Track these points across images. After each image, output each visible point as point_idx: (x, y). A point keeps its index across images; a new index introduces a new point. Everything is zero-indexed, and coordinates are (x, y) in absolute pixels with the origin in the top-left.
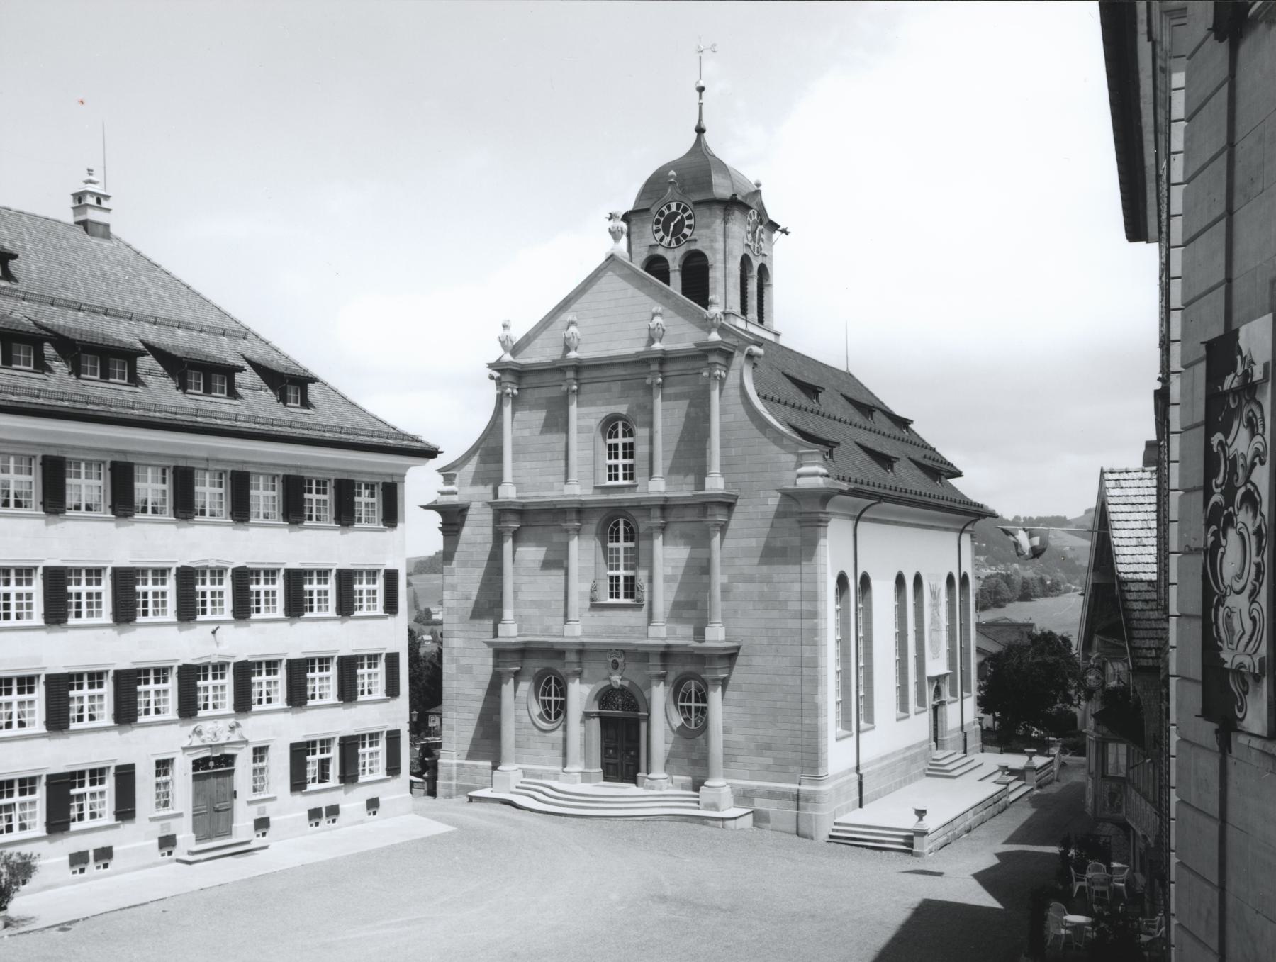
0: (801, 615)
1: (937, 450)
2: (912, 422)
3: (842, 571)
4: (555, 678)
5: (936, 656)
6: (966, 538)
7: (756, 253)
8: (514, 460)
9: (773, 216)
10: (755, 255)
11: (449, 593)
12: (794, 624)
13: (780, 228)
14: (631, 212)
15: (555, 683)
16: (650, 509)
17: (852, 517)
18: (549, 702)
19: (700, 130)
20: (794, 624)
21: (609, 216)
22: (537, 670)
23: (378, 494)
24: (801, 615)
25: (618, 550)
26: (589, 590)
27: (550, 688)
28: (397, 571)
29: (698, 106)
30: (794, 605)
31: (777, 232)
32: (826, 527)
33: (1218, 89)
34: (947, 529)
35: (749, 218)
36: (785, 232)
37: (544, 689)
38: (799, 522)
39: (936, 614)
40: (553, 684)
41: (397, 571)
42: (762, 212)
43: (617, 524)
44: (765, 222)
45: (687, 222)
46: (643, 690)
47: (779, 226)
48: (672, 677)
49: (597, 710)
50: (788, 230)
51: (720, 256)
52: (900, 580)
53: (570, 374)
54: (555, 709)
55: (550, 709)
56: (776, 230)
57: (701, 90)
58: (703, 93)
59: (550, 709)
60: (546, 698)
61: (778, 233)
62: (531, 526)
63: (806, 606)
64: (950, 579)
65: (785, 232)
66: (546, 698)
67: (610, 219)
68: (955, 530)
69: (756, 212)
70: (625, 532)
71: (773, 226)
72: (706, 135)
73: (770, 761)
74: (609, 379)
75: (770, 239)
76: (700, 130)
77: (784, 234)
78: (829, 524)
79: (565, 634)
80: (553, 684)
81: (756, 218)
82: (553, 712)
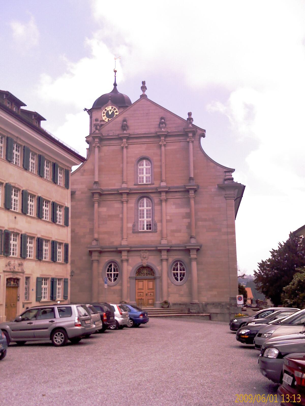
0: (227, 233)
2: (233, 171)
12: (224, 237)
16: (161, 193)
18: (177, 274)
19: (115, 85)
20: (224, 237)
22: (107, 260)
24: (227, 233)
25: (143, 210)
26: (132, 226)
30: (224, 230)
37: (108, 269)
38: (225, 198)
40: (179, 265)
45: (115, 111)
48: (171, 260)
49: (134, 276)
53: (125, 140)
55: (178, 277)
57: (115, 71)
62: (104, 201)
63: (229, 230)
76: (115, 85)
80: (179, 265)
82: (113, 279)
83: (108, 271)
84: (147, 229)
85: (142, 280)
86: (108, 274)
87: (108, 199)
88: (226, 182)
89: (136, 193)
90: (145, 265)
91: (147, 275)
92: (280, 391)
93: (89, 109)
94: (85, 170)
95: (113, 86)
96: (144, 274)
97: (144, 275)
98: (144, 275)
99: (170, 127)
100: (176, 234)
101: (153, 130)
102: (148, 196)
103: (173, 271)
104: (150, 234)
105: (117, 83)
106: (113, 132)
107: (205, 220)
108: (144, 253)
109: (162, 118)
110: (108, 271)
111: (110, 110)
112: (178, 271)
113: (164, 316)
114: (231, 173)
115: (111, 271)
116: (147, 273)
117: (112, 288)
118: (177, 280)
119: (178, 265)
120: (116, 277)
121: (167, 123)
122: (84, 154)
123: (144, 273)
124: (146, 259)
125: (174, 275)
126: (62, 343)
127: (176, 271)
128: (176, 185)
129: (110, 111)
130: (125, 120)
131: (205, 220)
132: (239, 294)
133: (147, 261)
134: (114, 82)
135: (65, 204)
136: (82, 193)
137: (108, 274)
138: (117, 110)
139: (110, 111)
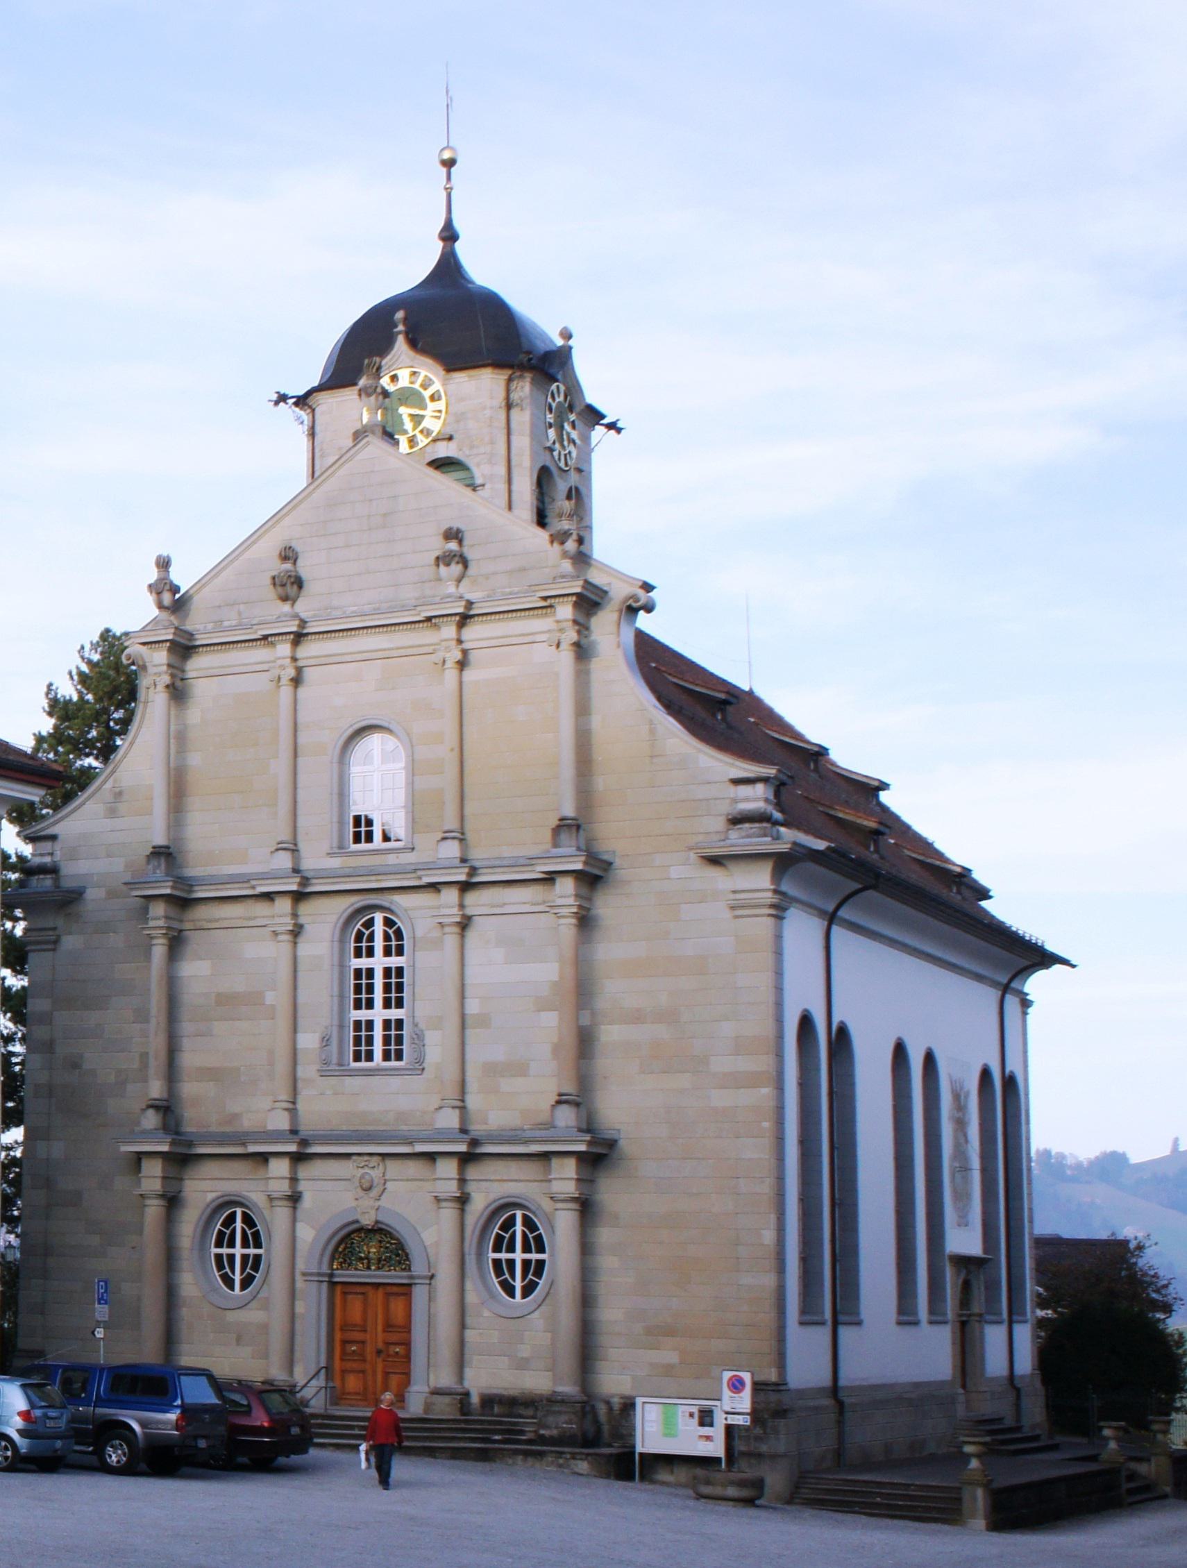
2: (884, 786)
3: (806, 1010)
5: (963, 1222)
7: (562, 464)
9: (592, 397)
10: (560, 469)
13: (605, 421)
17: (821, 913)
19: (449, 235)
21: (275, 397)
22: (210, 1196)
27: (234, 1232)
29: (444, 194)
31: (597, 427)
33: (596, 445)
34: (979, 978)
35: (550, 400)
39: (962, 1140)
42: (574, 389)
43: (370, 924)
44: (578, 408)
46: (419, 1229)
47: (602, 417)
50: (619, 425)
52: (900, 1051)
56: (598, 424)
57: (449, 164)
58: (453, 170)
59: (233, 1271)
61: (599, 431)
64: (986, 1074)
65: (164, 564)
67: (277, 403)
68: (994, 984)
69: (562, 388)
70: (387, 937)
71: (594, 416)
72: (458, 245)
73: (672, 1357)
74: (359, 657)
75: (586, 439)
76: (449, 235)
77: (612, 432)
81: (562, 398)
84: (387, 1056)
85: (359, 1289)
87: (217, 920)
90: (367, 1221)
91: (378, 1268)
92: (523, 1428)
93: (301, 392)
94: (120, 794)
95: (439, 246)
96: (369, 1262)
97: (369, 1268)
98: (369, 1268)
99: (487, 577)
100: (507, 1085)
101: (409, 594)
102: (386, 904)
104: (395, 1082)
105: (457, 225)
106: (240, 613)
107: (637, 1017)
108: (366, 1170)
109: (453, 535)
110: (219, 1244)
111: (417, 419)
115: (245, 1258)
116: (379, 1260)
117: (232, 1317)
119: (514, 1225)
120: (252, 1269)
121: (469, 553)
123: (367, 1258)
124: (374, 1193)
126: (8, 1465)
128: (508, 852)
129: (412, 416)
130: (288, 555)
131: (637, 1017)
133: (378, 1204)
134: (441, 224)
136: (112, 894)
137: (219, 1257)
138: (437, 386)
139: (412, 416)
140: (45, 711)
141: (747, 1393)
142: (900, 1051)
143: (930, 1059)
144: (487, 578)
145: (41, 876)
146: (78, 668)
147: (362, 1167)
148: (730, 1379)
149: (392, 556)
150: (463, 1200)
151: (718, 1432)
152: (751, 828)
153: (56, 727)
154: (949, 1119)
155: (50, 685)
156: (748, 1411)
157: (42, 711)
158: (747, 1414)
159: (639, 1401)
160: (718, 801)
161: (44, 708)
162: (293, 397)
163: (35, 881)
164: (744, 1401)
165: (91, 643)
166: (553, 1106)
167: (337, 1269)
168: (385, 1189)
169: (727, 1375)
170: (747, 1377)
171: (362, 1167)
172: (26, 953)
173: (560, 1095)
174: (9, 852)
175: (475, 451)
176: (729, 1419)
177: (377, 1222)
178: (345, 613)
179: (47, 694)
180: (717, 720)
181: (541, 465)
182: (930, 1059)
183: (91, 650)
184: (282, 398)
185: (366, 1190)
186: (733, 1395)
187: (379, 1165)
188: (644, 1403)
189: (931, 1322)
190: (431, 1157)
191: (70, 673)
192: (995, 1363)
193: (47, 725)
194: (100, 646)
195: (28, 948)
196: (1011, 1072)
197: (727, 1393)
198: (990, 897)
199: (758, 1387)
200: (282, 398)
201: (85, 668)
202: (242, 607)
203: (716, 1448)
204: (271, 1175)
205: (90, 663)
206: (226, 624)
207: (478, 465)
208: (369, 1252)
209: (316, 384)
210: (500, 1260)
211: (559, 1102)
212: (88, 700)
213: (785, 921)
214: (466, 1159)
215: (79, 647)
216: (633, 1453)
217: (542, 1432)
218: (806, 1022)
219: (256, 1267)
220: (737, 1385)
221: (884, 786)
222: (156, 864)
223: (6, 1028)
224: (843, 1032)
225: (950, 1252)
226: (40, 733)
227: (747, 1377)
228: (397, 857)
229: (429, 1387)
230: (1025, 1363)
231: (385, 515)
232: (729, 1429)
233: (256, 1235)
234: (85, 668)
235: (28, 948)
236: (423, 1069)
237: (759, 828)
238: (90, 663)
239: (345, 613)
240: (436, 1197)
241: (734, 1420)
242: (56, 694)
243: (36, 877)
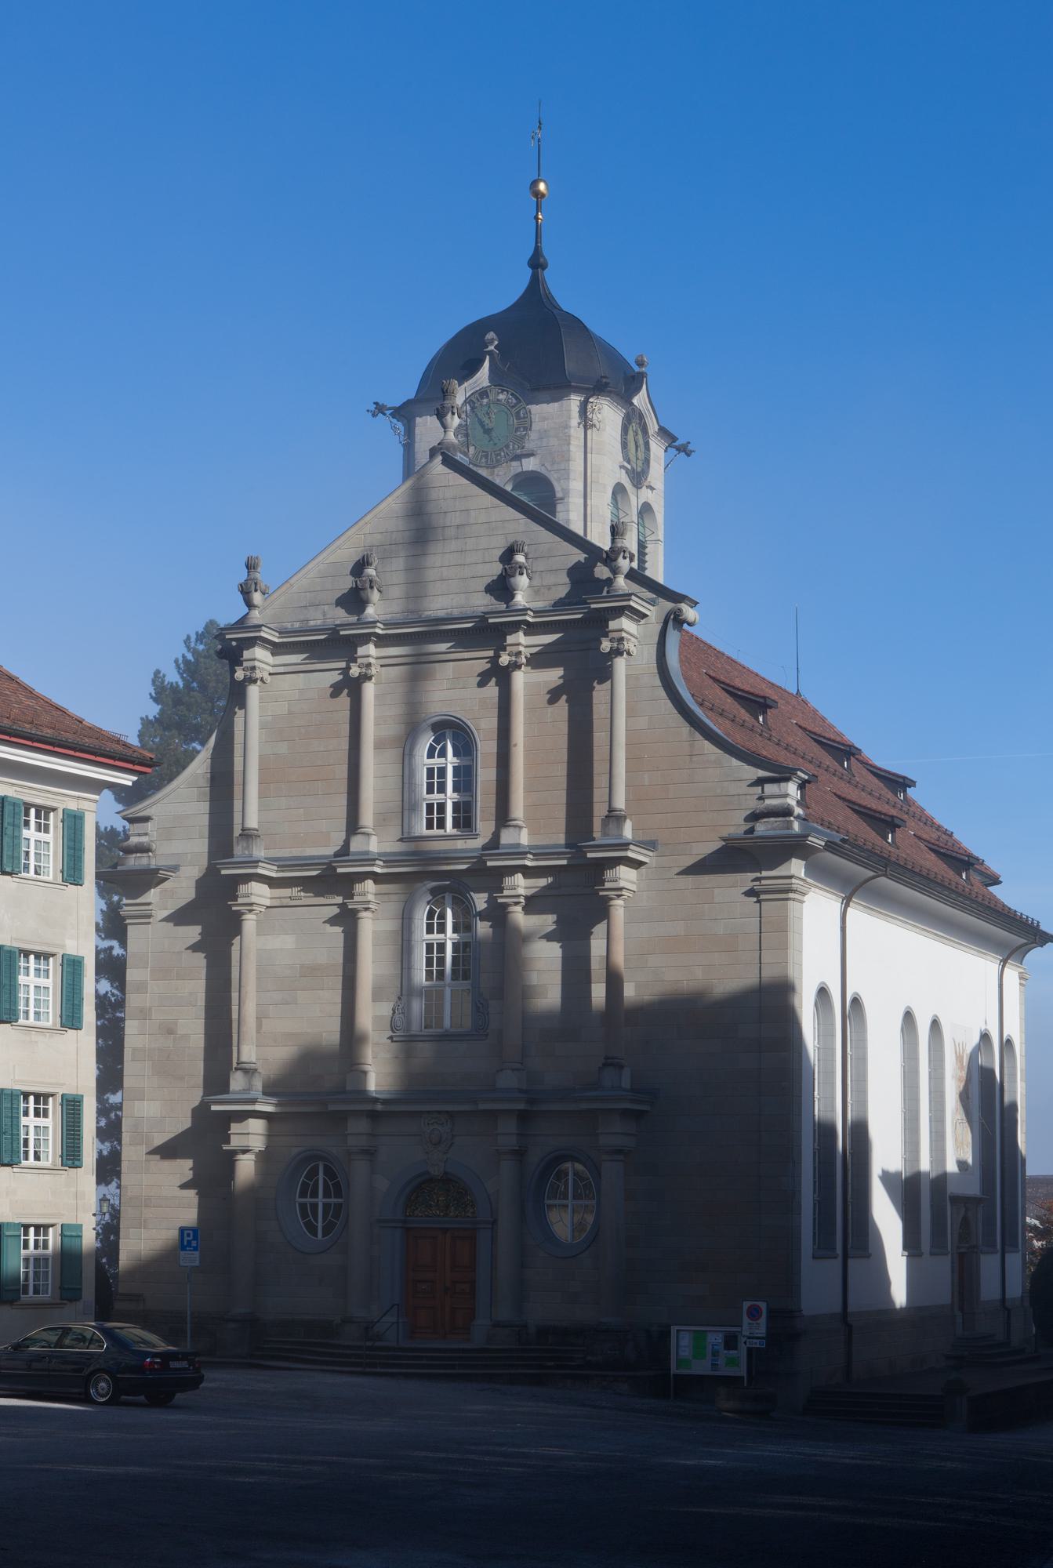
1: (955, 836)
2: (912, 784)
4: (325, 1166)
6: (1012, 974)
8: (262, 795)
11: (135, 1023)
14: (408, 403)
15: (325, 1173)
19: (537, 263)
21: (373, 407)
23: (56, 827)
28: (83, 957)
32: (802, 902)
36: (689, 443)
41: (83, 957)
51: (576, 485)
52: (909, 1017)
54: (324, 1219)
55: (316, 1220)
60: (308, 1200)
66: (308, 1200)
76: (537, 263)
77: (683, 454)
78: (806, 898)
79: (348, 1088)
83: (303, 1194)
86: (303, 1206)
88: (761, 828)
89: (82, 758)
93: (398, 404)
95: (529, 272)
103: (300, 1197)
105: (546, 251)
106: (324, 614)
110: (303, 1194)
112: (317, 1197)
113: (401, 1374)
114: (783, 785)
118: (313, 1229)
119: (323, 1227)
122: (991, 889)
125: (304, 1215)
127: (311, 1197)
132: (770, 1311)
135: (63, 946)
137: (303, 1206)
140: (152, 697)
141: (763, 1320)
142: (909, 1017)
143: (935, 1024)
144: (549, 589)
145: (138, 855)
146: (184, 656)
147: (432, 1124)
148: (749, 1308)
149: (14, 818)
150: (520, 1154)
151: (742, 1353)
152: (776, 822)
153: (162, 712)
154: (953, 1077)
155: (157, 672)
156: (764, 1335)
157: (149, 697)
158: (763, 1338)
159: (674, 1329)
160: (748, 797)
161: (150, 694)
162: (389, 409)
163: (133, 860)
164: (761, 1327)
165: (197, 633)
166: (599, 1068)
167: (410, 1216)
168: (452, 1143)
169: (746, 1305)
170: (763, 1305)
171: (432, 1124)
172: (126, 925)
173: (607, 1058)
174: (118, 830)
175: (556, 467)
176: (748, 1343)
177: (446, 1173)
178: (420, 617)
179: (154, 682)
180: (758, 721)
181: (617, 481)
182: (935, 1024)
183: (197, 641)
184: (380, 409)
185: (435, 1144)
186: (751, 1322)
187: (447, 1121)
188: (678, 1331)
189: (932, 1254)
190: (493, 1114)
191: (176, 661)
192: (989, 1289)
193: (153, 710)
194: (205, 637)
195: (128, 921)
196: (1009, 1036)
197: (746, 1320)
198: (1000, 882)
199: (773, 1315)
200: (380, 409)
201: (190, 657)
202: (326, 607)
203: (742, 1371)
204: (349, 1132)
205: (195, 652)
206: (312, 623)
207: (559, 480)
208: (438, 1201)
209: (412, 396)
210: (335, 1197)
211: (605, 1065)
212: (194, 687)
213: (804, 904)
214: (523, 1117)
215: (185, 638)
216: (670, 1373)
217: (589, 1358)
218: (823, 992)
219: (337, 1215)
220: (754, 1313)
221: (912, 784)
222: (245, 845)
223: (113, 995)
224: (856, 1001)
225: (951, 1193)
226: (147, 717)
227: (763, 1305)
228: (465, 842)
229: (491, 1320)
230: (1016, 1288)
231: (458, 526)
232: (750, 1350)
233: (337, 1186)
234: (190, 657)
235: (128, 921)
236: (487, 1035)
237: (784, 821)
238: (195, 652)
239: (420, 617)
240: (497, 1150)
241: (756, 1344)
242: (163, 681)
243: (134, 855)
